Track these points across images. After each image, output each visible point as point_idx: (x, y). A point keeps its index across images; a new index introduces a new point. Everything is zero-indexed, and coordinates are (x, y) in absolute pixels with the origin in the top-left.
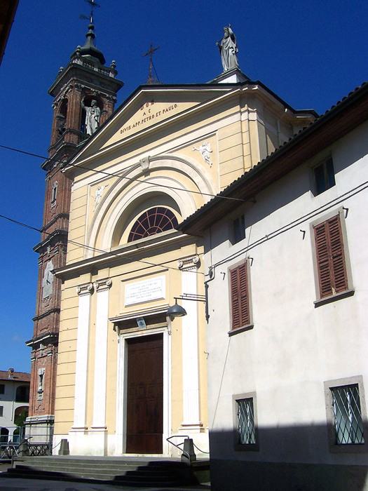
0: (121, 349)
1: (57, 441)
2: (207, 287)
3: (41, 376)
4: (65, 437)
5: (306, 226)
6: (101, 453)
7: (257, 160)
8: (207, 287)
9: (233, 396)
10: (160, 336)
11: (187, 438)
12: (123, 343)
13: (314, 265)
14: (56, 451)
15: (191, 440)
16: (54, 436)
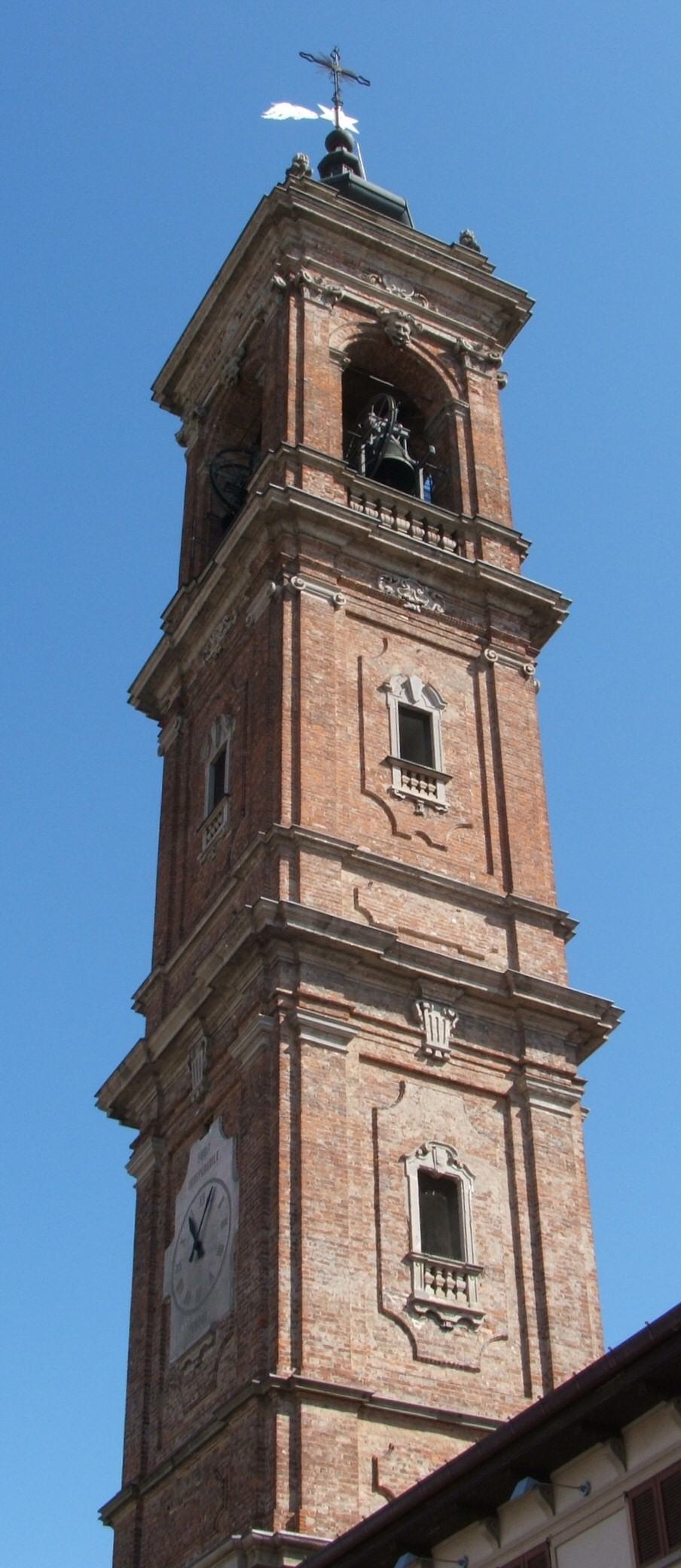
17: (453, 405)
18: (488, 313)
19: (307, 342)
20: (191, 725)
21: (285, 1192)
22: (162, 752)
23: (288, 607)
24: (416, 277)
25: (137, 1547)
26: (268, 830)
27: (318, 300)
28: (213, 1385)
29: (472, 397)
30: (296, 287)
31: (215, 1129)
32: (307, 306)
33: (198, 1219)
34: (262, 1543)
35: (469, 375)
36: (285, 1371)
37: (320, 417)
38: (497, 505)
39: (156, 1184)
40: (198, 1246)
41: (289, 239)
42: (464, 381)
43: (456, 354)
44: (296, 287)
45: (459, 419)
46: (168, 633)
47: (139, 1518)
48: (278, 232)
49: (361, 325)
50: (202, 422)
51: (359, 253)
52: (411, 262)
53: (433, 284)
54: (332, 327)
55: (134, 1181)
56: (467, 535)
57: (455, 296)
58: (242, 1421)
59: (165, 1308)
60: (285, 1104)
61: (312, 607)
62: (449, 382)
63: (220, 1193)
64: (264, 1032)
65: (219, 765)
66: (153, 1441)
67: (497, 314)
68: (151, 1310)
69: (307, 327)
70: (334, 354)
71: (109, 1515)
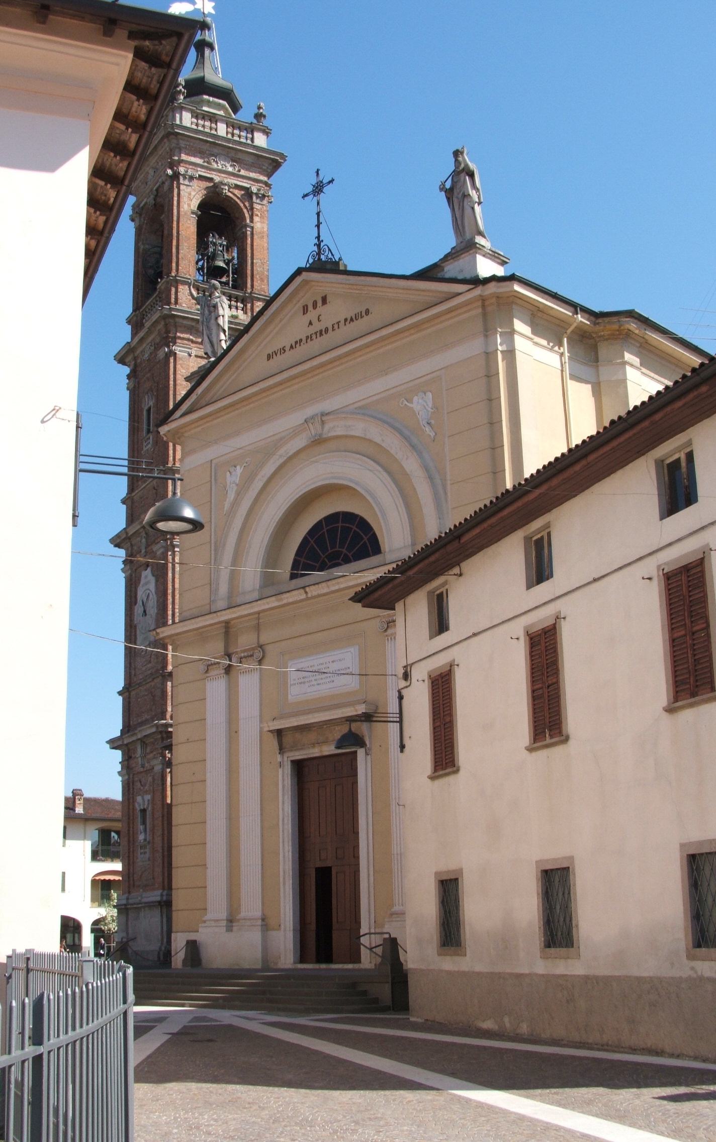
0: (284, 779)
1: (179, 941)
2: (401, 698)
3: (144, 811)
4: (192, 936)
5: (518, 628)
6: (139, 1089)
7: (594, 432)
8: (401, 698)
9: (436, 873)
10: (356, 752)
11: (387, 936)
12: (288, 768)
13: (561, 644)
14: (178, 958)
15: (395, 939)
16: (173, 935)
17: (246, 226)
18: (266, 166)
19: (181, 209)
20: (139, 383)
21: (170, 607)
22: (128, 389)
23: (172, 360)
24: (232, 154)
25: (129, 707)
26: (164, 466)
27: (187, 182)
28: (150, 662)
29: (256, 219)
30: (176, 176)
31: (149, 569)
32: (182, 187)
33: (145, 600)
34: (163, 725)
35: (255, 206)
36: (170, 465)
37: (186, 228)
38: (262, 280)
39: (131, 580)
40: (145, 611)
41: (173, 145)
42: (252, 209)
43: (248, 194)
44: (176, 176)
45: (249, 233)
46: (131, 518)
47: (129, 698)
48: (169, 140)
49: (207, 188)
50: (140, 215)
51: (205, 147)
52: (230, 148)
53: (240, 156)
54: (193, 193)
55: (127, 370)
56: (248, 300)
57: (250, 159)
58: (158, 680)
59: (135, 626)
60: (170, 575)
61: (181, 359)
62: (245, 211)
63: (151, 596)
64: (163, 547)
65: (149, 411)
66: (133, 673)
67: (270, 164)
68: (131, 626)
69: (181, 200)
70: (193, 213)
71: (124, 502)
